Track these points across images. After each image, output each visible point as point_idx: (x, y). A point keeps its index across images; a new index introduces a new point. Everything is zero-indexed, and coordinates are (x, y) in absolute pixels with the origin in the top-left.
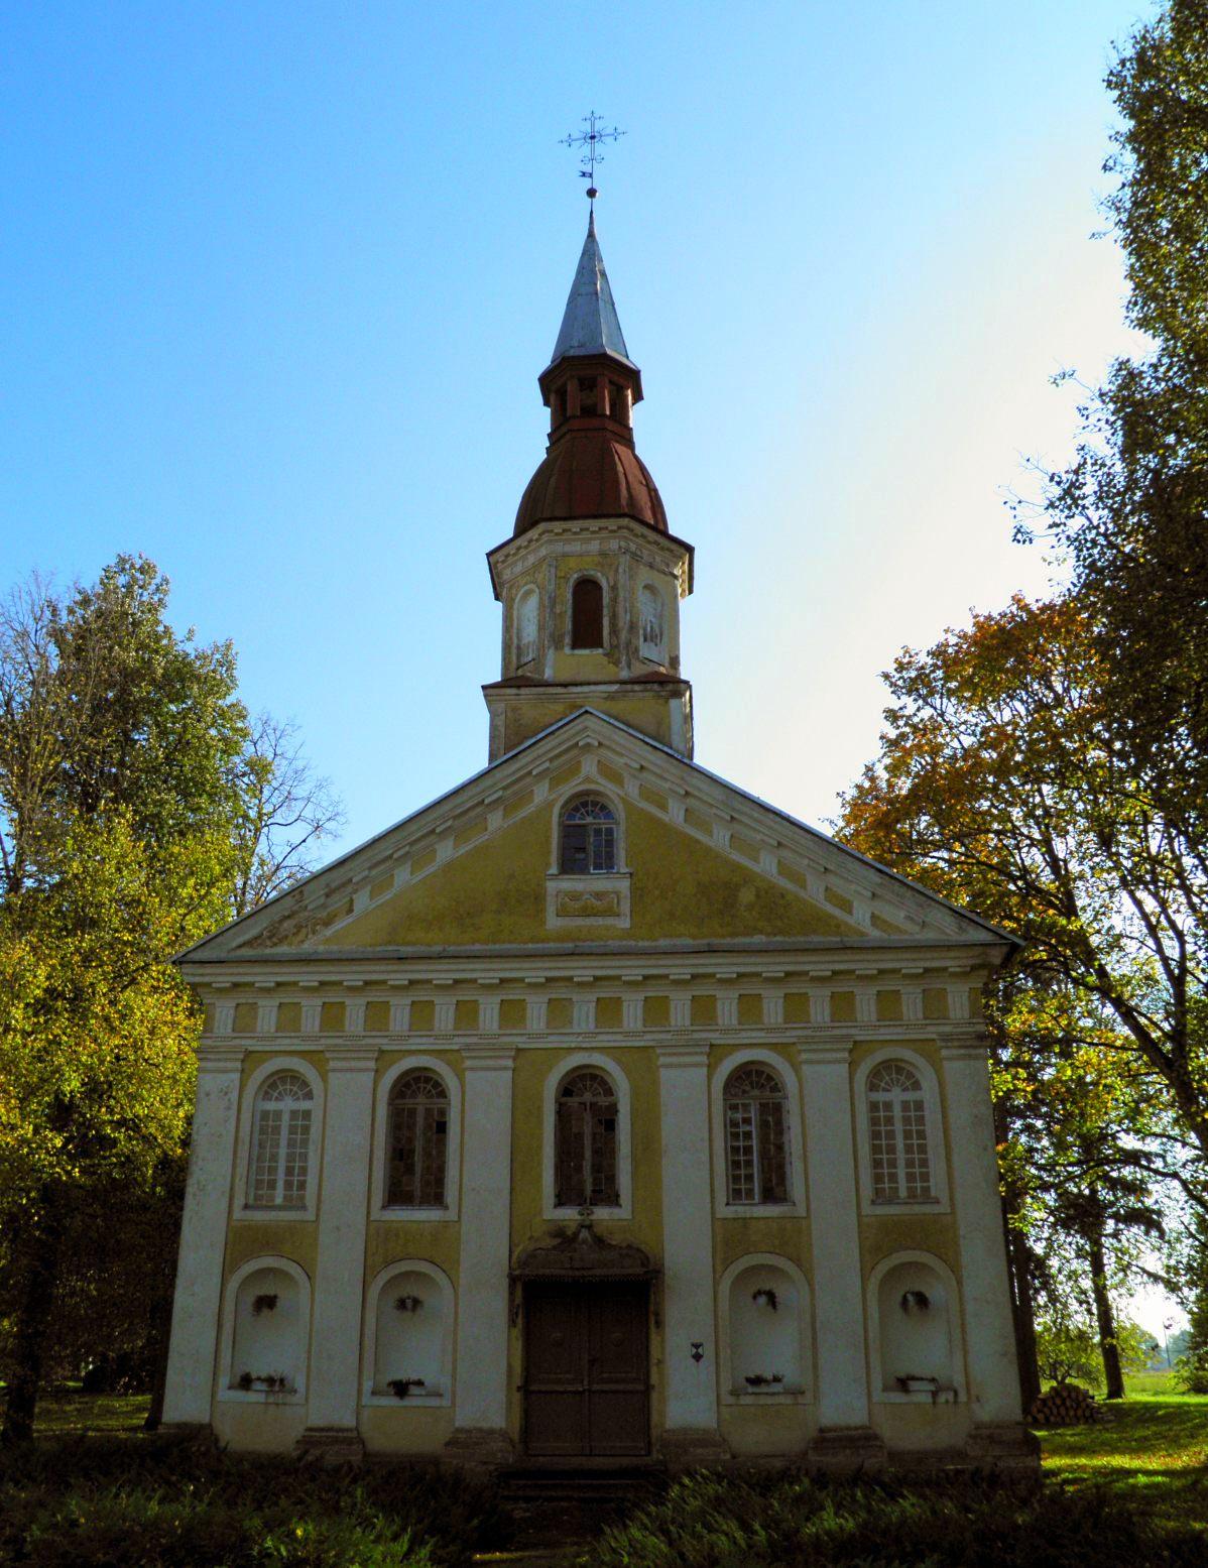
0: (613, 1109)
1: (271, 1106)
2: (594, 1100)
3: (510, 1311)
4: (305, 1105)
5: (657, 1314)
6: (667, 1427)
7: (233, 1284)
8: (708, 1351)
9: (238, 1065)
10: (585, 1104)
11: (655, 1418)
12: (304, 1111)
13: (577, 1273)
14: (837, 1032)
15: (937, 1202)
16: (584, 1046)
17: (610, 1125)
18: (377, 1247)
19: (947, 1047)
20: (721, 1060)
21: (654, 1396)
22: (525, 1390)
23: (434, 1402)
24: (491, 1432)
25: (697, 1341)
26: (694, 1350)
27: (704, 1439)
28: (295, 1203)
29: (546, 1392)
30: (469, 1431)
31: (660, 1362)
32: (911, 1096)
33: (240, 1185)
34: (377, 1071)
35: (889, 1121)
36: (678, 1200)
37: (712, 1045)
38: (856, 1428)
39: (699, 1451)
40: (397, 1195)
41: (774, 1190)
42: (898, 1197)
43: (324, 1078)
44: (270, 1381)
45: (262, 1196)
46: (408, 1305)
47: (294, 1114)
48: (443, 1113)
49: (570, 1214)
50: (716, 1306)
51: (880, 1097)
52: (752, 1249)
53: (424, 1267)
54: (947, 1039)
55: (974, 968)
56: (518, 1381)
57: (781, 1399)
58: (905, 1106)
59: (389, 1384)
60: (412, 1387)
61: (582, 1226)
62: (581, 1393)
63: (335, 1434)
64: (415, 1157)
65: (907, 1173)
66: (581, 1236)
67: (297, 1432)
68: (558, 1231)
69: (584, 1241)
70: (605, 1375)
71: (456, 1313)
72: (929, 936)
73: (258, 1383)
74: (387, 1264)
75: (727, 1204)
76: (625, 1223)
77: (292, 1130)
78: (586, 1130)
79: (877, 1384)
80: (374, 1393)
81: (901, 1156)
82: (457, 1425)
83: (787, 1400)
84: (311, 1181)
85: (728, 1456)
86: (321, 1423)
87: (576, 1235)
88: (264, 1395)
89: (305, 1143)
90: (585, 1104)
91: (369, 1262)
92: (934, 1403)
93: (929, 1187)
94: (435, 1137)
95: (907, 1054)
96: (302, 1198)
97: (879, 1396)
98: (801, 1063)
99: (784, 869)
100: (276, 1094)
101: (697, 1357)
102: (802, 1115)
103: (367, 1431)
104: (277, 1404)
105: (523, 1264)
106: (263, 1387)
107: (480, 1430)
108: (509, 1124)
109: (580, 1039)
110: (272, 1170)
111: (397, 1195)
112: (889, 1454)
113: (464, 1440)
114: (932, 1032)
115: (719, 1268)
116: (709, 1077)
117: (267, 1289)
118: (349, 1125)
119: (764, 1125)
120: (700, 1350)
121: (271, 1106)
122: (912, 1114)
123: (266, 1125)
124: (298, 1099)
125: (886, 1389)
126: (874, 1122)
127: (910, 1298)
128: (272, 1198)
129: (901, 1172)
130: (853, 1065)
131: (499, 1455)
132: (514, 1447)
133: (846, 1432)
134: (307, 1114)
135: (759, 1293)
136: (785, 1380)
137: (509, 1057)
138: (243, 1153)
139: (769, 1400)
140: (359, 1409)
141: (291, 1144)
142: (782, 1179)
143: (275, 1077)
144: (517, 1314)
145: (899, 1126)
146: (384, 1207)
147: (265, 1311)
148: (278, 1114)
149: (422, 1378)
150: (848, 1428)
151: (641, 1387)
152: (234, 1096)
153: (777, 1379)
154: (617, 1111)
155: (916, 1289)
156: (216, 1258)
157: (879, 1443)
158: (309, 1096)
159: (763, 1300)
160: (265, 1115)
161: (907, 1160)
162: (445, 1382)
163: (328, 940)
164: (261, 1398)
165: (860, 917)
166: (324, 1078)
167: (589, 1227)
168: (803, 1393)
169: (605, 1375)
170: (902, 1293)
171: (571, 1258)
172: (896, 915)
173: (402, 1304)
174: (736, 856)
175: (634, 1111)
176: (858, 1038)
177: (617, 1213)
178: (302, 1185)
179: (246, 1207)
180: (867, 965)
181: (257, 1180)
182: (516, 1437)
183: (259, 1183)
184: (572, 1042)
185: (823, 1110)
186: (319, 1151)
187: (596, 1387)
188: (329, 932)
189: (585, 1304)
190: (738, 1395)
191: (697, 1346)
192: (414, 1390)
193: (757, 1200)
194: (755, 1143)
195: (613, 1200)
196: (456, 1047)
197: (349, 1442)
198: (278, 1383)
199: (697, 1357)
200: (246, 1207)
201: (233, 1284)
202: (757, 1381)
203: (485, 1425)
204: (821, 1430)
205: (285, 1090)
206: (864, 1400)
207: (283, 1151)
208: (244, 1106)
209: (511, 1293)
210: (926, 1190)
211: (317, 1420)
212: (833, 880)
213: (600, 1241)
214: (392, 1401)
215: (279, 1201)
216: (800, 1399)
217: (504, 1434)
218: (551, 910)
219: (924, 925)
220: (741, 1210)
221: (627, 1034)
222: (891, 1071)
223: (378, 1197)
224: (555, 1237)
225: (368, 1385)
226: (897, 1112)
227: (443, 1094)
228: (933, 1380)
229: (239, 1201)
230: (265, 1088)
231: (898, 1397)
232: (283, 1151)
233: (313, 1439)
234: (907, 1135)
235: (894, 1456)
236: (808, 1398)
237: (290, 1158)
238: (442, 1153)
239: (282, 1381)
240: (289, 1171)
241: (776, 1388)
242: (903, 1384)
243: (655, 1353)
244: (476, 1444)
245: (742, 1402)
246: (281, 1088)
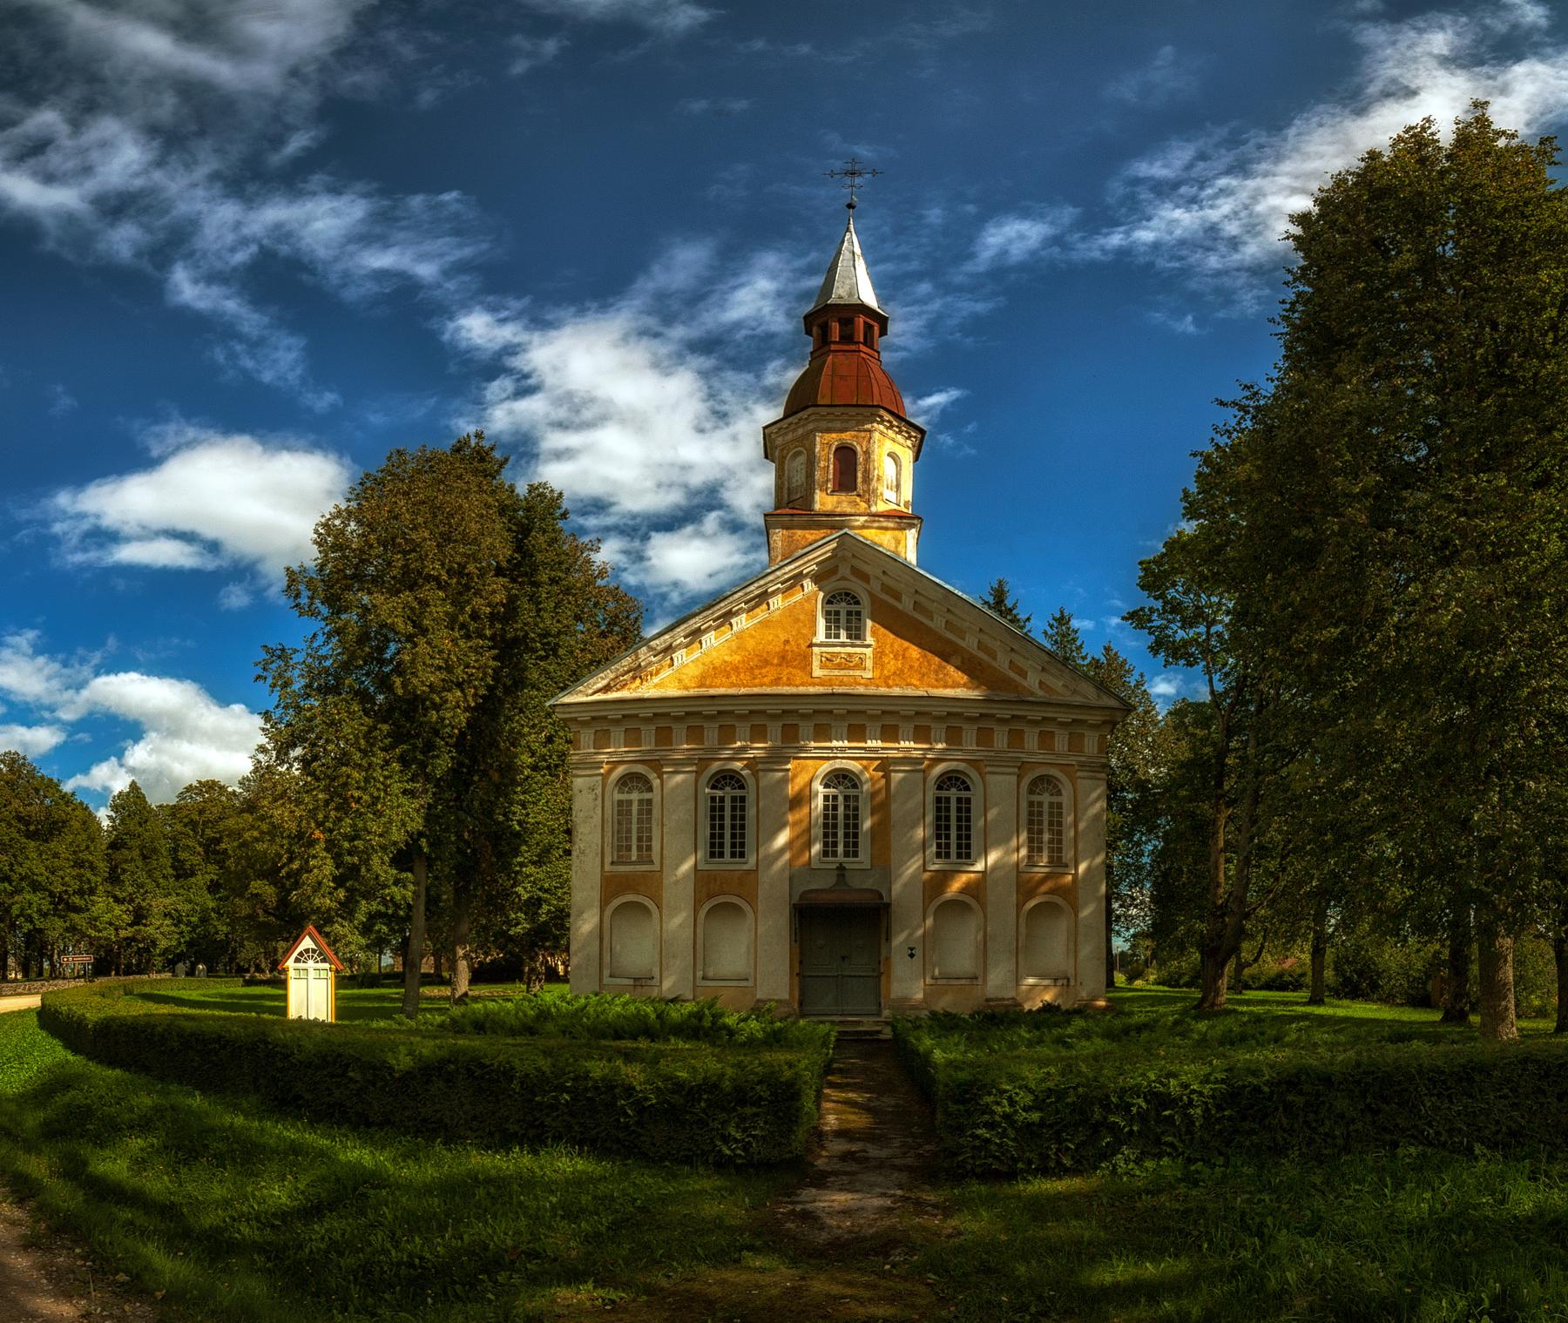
4: (647, 796)
7: (608, 913)
8: (918, 952)
32: (1055, 799)
33: (608, 850)
35: (1040, 814)
47: (1051, 805)
51: (1036, 798)
53: (735, 900)
54: (1082, 765)
55: (1104, 722)
72: (1078, 700)
84: (656, 845)
89: (649, 820)
95: (1053, 772)
99: (981, 646)
101: (912, 956)
110: (628, 839)
114: (1072, 760)
123: (623, 808)
126: (1031, 814)
134: (649, 802)
138: (608, 829)
141: (640, 821)
152: (599, 791)
156: (596, 895)
163: (656, 686)
165: (1032, 681)
166: (660, 777)
172: (1057, 684)
174: (949, 635)
178: (649, 848)
180: (1036, 714)
188: (656, 680)
199: (912, 956)
200: (612, 863)
201: (608, 913)
207: (634, 827)
212: (1015, 657)
218: (816, 663)
219: (1074, 692)
222: (1044, 783)
226: (1046, 806)
229: (608, 860)
232: (634, 827)
236: (980, 982)
237: (640, 830)
240: (640, 839)
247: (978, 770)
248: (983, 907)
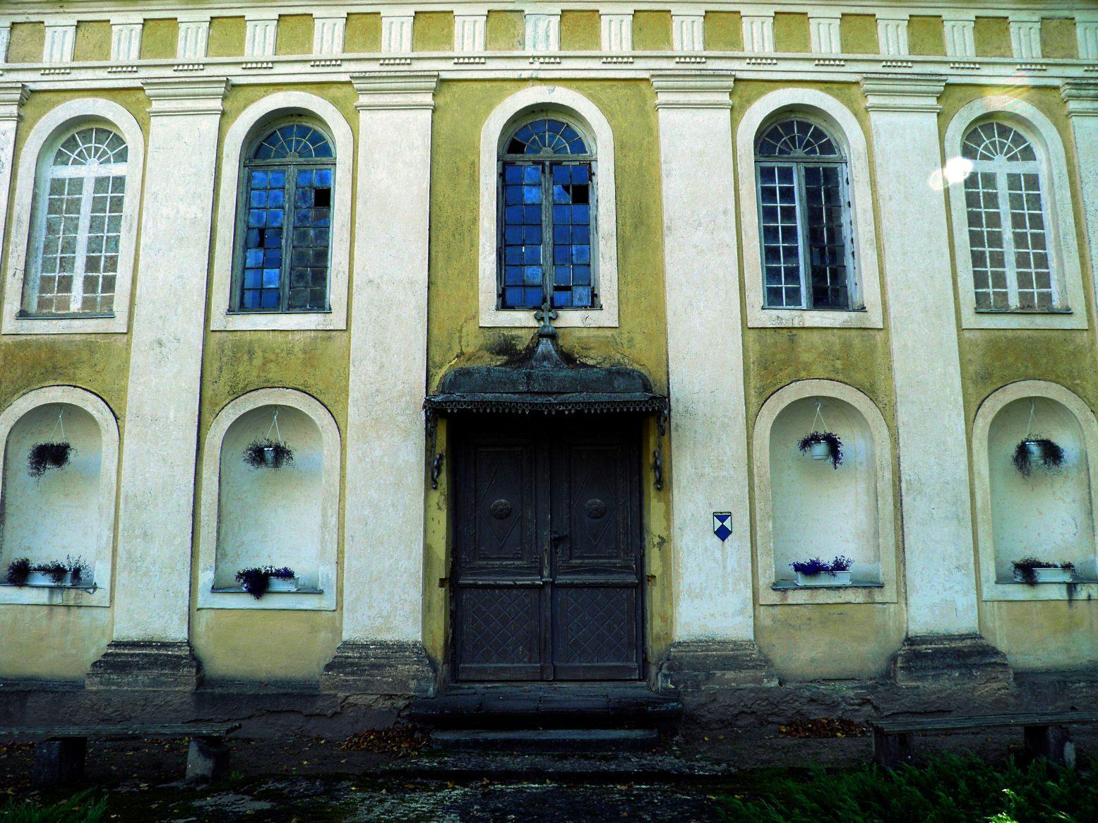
0: (587, 171)
1: (67, 172)
2: (557, 157)
3: (428, 464)
4: (115, 170)
5: (658, 468)
6: (677, 639)
8: (740, 525)
9: (14, 109)
10: (542, 163)
11: (655, 626)
12: (115, 178)
13: (540, 400)
14: (918, 69)
15: (1067, 312)
16: (542, 75)
17: (581, 194)
18: (221, 369)
19: (1078, 97)
20: (749, 102)
21: (654, 594)
22: (452, 583)
23: (309, 602)
24: (401, 647)
25: (723, 508)
26: (718, 524)
27: (729, 656)
28: (96, 308)
29: (484, 587)
30: (365, 646)
31: (663, 541)
32: (1021, 168)
34: (223, 113)
36: (693, 297)
37: (736, 80)
38: (962, 637)
39: (730, 675)
40: (251, 297)
41: (830, 290)
42: (1008, 306)
43: (144, 126)
44: (57, 572)
45: (51, 300)
46: (269, 457)
47: (100, 183)
48: (324, 178)
49: (523, 319)
50: (750, 457)
52: (803, 374)
56: (440, 571)
57: (850, 596)
58: (1013, 180)
59: (240, 576)
60: (274, 580)
61: (541, 336)
62: (541, 587)
63: (155, 652)
64: (283, 227)
65: (1019, 274)
66: (541, 349)
67: (94, 651)
68: (505, 347)
69: (546, 357)
70: (575, 562)
71: (343, 467)
73: (39, 575)
74: (237, 393)
75: (763, 308)
76: (609, 333)
77: (98, 205)
78: (544, 186)
79: (989, 571)
80: (215, 589)
81: (1009, 250)
82: (346, 636)
83: (857, 597)
85: (775, 683)
86: (134, 634)
87: (531, 350)
88: (46, 593)
89: (115, 223)
90: (542, 163)
91: (208, 393)
92: (1070, 601)
93: (1050, 295)
94: (312, 213)
96: (110, 301)
97: (992, 590)
98: (866, 109)
100: (74, 156)
101: (723, 533)
102: (873, 183)
103: (204, 645)
104: (69, 606)
105: (451, 384)
106: (46, 580)
107: (382, 645)
108: (426, 185)
109: (537, 65)
110: (67, 263)
111: (251, 297)
112: (1015, 674)
113: (356, 661)
115: (753, 400)
116: (734, 123)
117: (54, 437)
118: (179, 188)
119: (812, 196)
120: (727, 524)
121: (67, 172)
122: (1024, 192)
123: (61, 198)
124: (108, 161)
125: (1001, 580)
127: (1034, 449)
128: (65, 304)
129: (1011, 272)
130: (943, 118)
131: (413, 684)
132: (435, 671)
133: (947, 645)
134: (119, 182)
135: (806, 443)
136: (852, 569)
137: (426, 90)
139: (832, 597)
140: (192, 611)
141: (95, 225)
142: (839, 273)
143: (74, 132)
144: (439, 468)
145: (1005, 209)
146: (231, 311)
147: (51, 471)
148: (77, 184)
149: (291, 566)
150: (950, 638)
151: (632, 579)
153: (839, 566)
154: (592, 174)
155: (1044, 437)
157: (998, 660)
158: (122, 157)
159: (820, 449)
160: (57, 186)
161: (1019, 255)
162: (324, 572)
164: (42, 597)
166: (144, 126)
167: (553, 337)
168: (881, 586)
169: (575, 562)
170: (1023, 437)
171: (529, 376)
173: (257, 456)
175: (619, 172)
176: (951, 80)
177: (595, 318)
178: (109, 284)
179: (23, 315)
181: (43, 278)
182: (439, 656)
183: (46, 283)
184: (522, 69)
185: (903, 184)
186: (134, 232)
187: (563, 579)
189: (546, 452)
190: (785, 590)
191: (722, 517)
192: (278, 584)
193: (804, 306)
194: (800, 224)
195: (593, 302)
196: (345, 78)
197: (175, 663)
198: (69, 576)
199: (723, 533)
202: (812, 569)
203: (388, 637)
204: (910, 641)
205: (97, 150)
206: (973, 597)
207: (83, 236)
208: (21, 171)
209: (430, 434)
210: (1046, 298)
211: (127, 629)
213: (568, 358)
214: (246, 601)
215: (75, 306)
216: (878, 597)
217: (420, 652)
220: (786, 316)
221: (608, 59)
223: (221, 298)
224: (498, 353)
225: (206, 578)
227: (325, 150)
228: (1067, 567)
230: (58, 146)
231: (1019, 592)
232: (83, 236)
233: (122, 659)
234: (1018, 221)
235: (1024, 677)
236: (889, 594)
237: (94, 244)
238: (323, 232)
239: (77, 572)
240: (92, 264)
241: (842, 579)
242: (1027, 571)
243: (655, 524)
244: (373, 666)
245: (790, 601)
246: (82, 147)
247: (849, 103)
248: (889, 412)
